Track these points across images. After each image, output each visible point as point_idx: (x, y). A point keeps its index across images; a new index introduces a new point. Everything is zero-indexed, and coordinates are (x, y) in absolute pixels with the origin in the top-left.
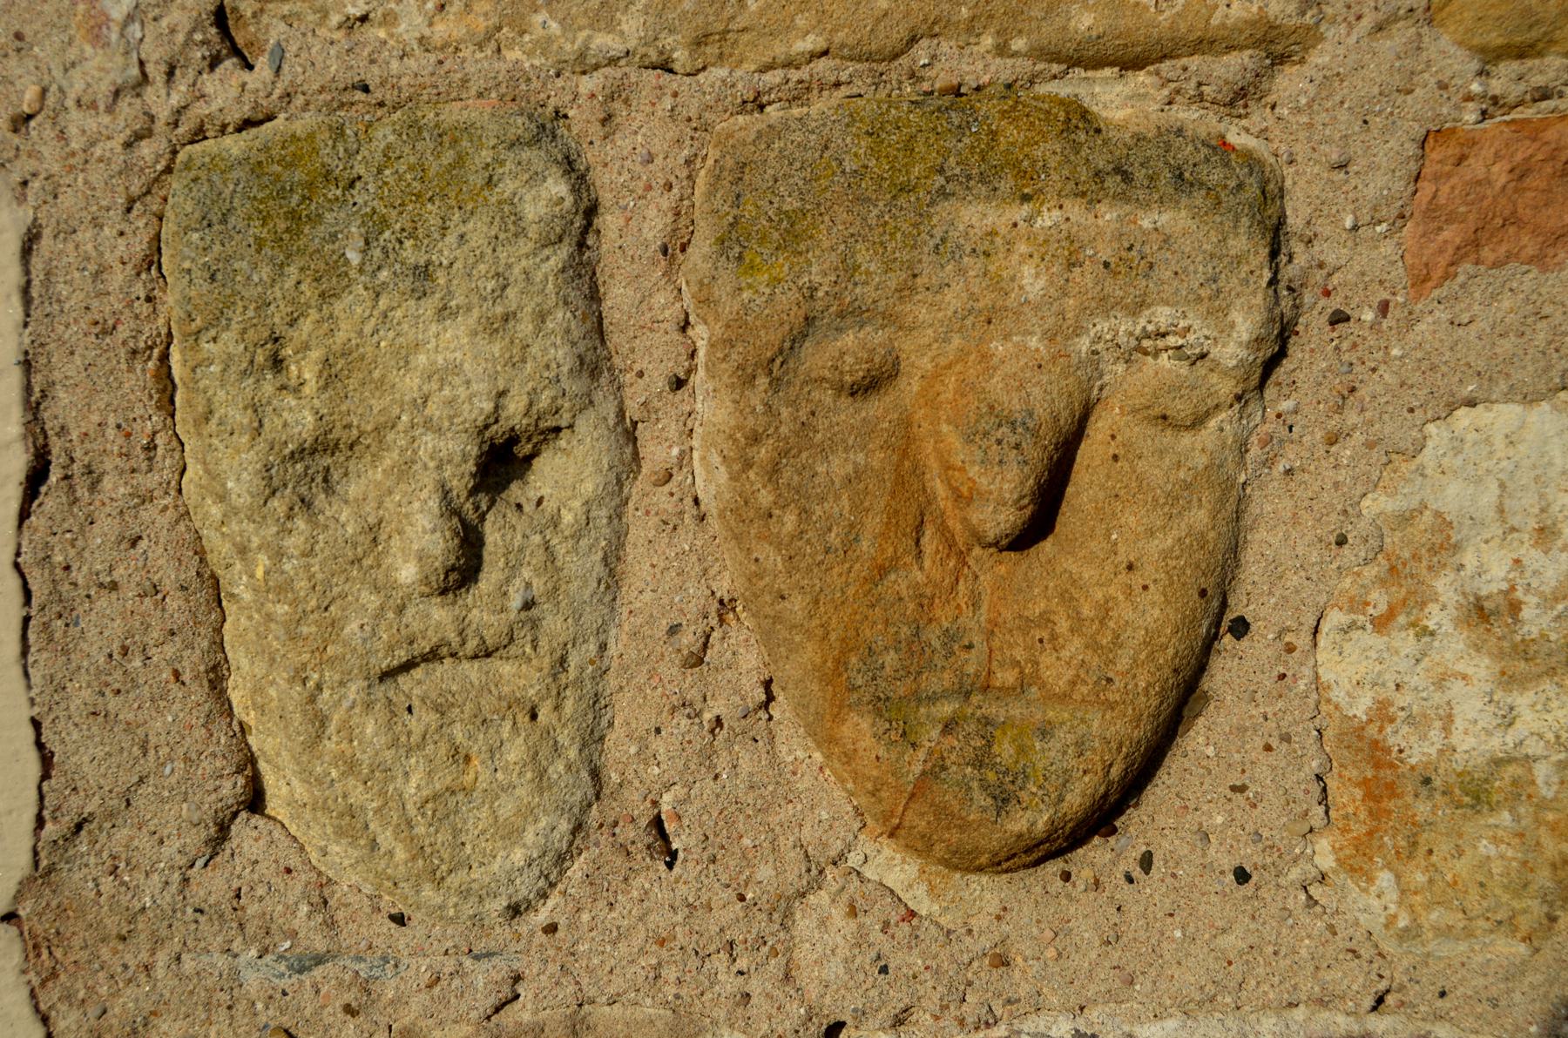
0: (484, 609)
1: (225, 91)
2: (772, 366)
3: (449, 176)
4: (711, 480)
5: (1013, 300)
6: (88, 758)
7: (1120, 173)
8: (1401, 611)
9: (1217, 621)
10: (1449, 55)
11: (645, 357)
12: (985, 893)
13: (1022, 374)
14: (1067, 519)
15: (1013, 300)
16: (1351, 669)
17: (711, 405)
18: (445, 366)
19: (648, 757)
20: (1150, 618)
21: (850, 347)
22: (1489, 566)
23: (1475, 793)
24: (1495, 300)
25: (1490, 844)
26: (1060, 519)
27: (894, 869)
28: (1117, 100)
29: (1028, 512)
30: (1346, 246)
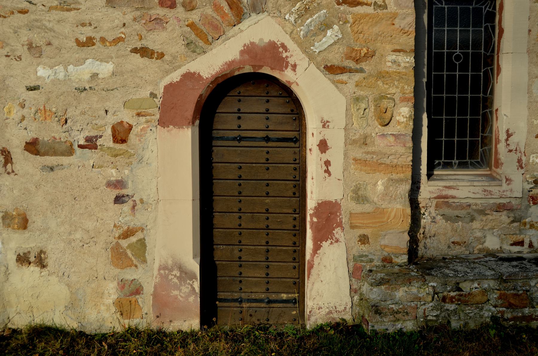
0: (364, 116)
1: (354, 95)
2: (376, 106)
3: (363, 99)
4: (373, 110)
5: (385, 103)
6: (348, 122)
7: (389, 99)
8: (400, 116)
9: (392, 116)
10: (401, 94)
11: (370, 106)
12: (383, 127)
13: (385, 106)
14: (390, 124)
15: (385, 103)
16: (398, 118)
17: (373, 107)
18: (363, 106)
19: (370, 122)
20: (390, 116)
21: (379, 105)
22: (403, 114)
23: (402, 123)
24: (403, 104)
25: (403, 125)
26: (414, 11)
27: (379, 127)
28: (388, 96)
29: (197, 122)
30: (397, 101)
